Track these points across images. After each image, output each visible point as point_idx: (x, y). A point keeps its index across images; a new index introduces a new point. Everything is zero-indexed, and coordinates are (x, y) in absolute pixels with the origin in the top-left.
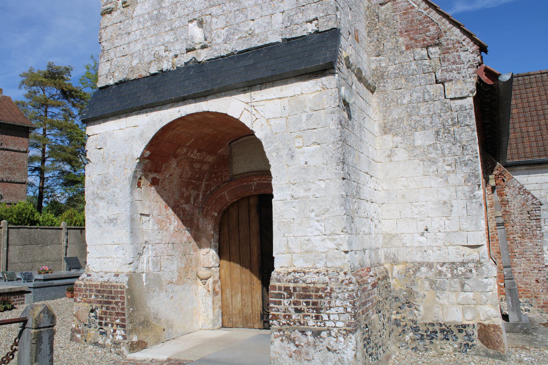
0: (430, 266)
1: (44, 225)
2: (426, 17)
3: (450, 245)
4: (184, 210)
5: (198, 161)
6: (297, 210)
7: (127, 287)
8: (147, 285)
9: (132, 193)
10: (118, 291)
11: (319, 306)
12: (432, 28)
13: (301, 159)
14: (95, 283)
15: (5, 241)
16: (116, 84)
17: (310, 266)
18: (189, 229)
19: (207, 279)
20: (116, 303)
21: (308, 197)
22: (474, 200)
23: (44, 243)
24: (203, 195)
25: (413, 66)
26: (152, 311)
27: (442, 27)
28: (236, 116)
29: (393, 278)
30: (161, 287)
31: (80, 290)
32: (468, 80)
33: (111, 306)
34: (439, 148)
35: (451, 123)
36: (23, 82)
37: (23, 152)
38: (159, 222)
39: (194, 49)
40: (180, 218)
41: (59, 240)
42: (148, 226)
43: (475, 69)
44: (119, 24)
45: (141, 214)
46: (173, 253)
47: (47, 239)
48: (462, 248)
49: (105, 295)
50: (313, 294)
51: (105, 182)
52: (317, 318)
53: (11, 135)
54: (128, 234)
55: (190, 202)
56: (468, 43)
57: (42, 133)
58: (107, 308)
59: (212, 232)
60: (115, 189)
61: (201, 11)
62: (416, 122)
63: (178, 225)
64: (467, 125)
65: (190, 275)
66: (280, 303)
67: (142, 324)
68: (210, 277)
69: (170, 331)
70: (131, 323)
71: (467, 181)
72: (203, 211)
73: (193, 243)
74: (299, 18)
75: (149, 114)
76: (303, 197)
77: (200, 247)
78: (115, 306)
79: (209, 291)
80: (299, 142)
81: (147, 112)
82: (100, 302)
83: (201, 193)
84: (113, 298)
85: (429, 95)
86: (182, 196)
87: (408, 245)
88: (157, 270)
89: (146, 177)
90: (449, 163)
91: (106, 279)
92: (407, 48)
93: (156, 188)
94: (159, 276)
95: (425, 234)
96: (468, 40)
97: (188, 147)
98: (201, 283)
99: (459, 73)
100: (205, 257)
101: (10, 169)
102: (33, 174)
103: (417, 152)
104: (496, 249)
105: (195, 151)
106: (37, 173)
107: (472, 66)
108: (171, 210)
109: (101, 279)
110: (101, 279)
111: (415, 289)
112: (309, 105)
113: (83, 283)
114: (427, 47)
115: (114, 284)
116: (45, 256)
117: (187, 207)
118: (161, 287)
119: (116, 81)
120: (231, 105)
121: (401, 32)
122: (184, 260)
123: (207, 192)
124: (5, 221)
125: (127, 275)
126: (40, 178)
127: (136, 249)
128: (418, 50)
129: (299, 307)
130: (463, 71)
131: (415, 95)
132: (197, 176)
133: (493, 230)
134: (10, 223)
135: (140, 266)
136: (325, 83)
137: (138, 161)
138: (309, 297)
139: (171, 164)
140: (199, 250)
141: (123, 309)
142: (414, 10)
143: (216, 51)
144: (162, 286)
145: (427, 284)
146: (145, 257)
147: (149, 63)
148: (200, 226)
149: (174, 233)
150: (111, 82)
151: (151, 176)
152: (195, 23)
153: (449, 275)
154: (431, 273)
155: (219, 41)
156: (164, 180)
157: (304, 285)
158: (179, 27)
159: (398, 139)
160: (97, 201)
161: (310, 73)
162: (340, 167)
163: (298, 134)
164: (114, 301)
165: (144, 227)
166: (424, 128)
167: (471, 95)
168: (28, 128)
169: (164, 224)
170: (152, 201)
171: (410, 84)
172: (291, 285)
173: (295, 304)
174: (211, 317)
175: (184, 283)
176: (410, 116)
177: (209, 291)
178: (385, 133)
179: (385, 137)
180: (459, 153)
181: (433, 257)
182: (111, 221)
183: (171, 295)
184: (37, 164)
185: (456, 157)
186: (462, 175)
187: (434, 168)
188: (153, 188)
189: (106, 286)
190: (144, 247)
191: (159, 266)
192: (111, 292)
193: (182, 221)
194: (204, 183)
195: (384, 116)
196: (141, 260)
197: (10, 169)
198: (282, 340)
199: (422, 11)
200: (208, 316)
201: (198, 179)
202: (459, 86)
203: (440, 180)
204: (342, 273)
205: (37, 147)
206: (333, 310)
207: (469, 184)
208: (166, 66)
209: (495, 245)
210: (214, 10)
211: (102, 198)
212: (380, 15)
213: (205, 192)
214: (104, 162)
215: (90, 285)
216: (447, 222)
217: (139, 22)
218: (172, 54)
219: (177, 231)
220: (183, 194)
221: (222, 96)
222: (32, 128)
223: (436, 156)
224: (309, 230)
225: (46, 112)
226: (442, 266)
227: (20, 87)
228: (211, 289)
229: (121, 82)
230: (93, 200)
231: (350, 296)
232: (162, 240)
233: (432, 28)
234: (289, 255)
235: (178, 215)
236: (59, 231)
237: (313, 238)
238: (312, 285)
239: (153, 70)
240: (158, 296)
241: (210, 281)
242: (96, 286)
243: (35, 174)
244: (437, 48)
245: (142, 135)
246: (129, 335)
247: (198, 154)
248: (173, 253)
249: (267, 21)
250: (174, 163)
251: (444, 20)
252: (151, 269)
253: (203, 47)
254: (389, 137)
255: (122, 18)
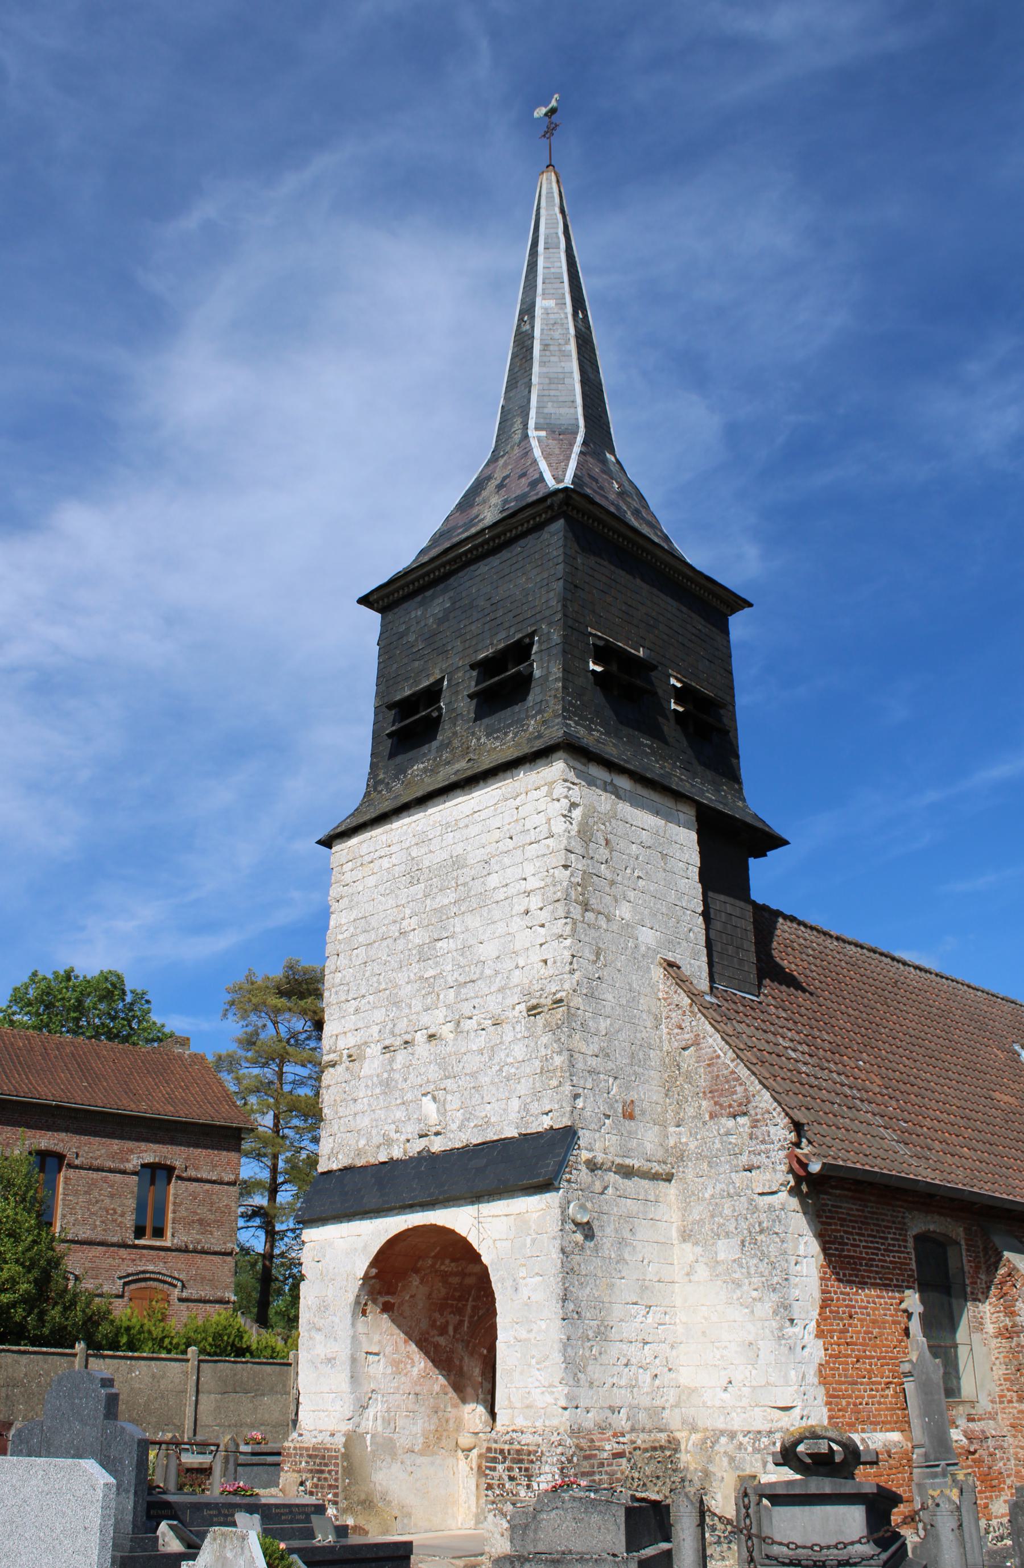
0: (732, 1435)
1: (259, 1358)
2: (733, 1072)
3: (756, 1405)
4: (436, 1346)
5: (456, 1274)
6: (519, 1355)
7: (343, 1450)
8: (372, 1451)
9: (353, 1325)
10: (332, 1456)
11: (530, 1473)
12: (739, 1089)
13: (525, 1292)
14: (306, 1445)
15: (194, 1384)
16: (340, 1170)
17: (530, 1424)
18: (444, 1372)
19: (470, 1450)
20: (329, 1472)
21: (529, 1340)
22: (783, 1342)
23: (258, 1390)
24: (469, 1322)
25: (718, 1145)
26: (378, 1487)
27: (751, 1089)
28: (464, 1234)
29: (687, 1452)
30: (394, 1455)
31: (289, 1455)
32: (778, 1168)
33: (324, 1476)
34: (745, 1265)
35: (758, 1229)
36: (232, 1003)
37: (229, 1184)
38: (395, 1364)
39: (426, 1135)
40: (429, 1358)
41: (284, 1386)
42: (378, 1369)
43: (786, 1152)
44: (344, 1085)
45: (367, 1353)
46: (416, 1407)
47: (264, 1383)
48: (769, 1410)
49: (318, 1461)
50: (525, 1457)
51: (323, 1308)
52: (529, 1486)
53: (206, 1147)
54: (348, 1379)
55: (447, 1332)
56: (779, 1114)
57: (271, 1125)
58: (319, 1479)
59: (480, 1379)
60: (334, 1318)
61: (435, 1082)
62: (720, 1226)
63: (425, 1367)
64: (777, 1233)
65: (444, 1443)
66: (494, 1469)
67: (362, 1503)
68: (474, 1448)
69: (405, 1521)
70: (345, 1499)
71: (775, 1313)
72: (467, 1346)
73: (452, 1394)
74: (535, 1108)
75: (373, 1221)
76: (525, 1340)
77: (464, 1401)
78: (327, 1475)
79: (472, 1469)
80: (523, 1272)
81: (371, 1218)
82: (311, 1471)
83: (466, 1319)
84: (326, 1465)
85: (734, 1188)
86: (433, 1324)
87: (709, 1404)
88: (388, 1431)
89: (374, 1301)
90: (756, 1287)
91: (319, 1439)
92: (711, 1117)
93: (390, 1317)
94: (391, 1439)
95: (729, 1389)
96: (779, 1109)
97: (434, 1257)
98: (462, 1457)
99: (768, 1157)
100: (470, 1416)
101: (201, 1222)
102: (250, 1224)
103: (720, 1269)
104: (1009, 1419)
105: (447, 1261)
106: (257, 1222)
107: (782, 1148)
108: (414, 1346)
109: (314, 1440)
110: (314, 1440)
111: (712, 1468)
112: (534, 1227)
113: (292, 1445)
114: (734, 1117)
115: (328, 1446)
116: (259, 1416)
117: (442, 1341)
118: (394, 1455)
119: (340, 1166)
120: (458, 1219)
121: (704, 1092)
122: (435, 1420)
123: (473, 1317)
124: (194, 1348)
125: (344, 1435)
126: (267, 1233)
127: (358, 1399)
128: (724, 1120)
129: (512, 1474)
130: (772, 1154)
131: (719, 1186)
132: (457, 1294)
133: (1002, 1382)
134: (202, 1351)
135: (363, 1424)
136: (549, 1200)
137: (361, 1282)
138: (521, 1461)
139: (411, 1282)
140: (461, 1405)
141: (336, 1480)
142: (720, 1061)
143: (451, 1140)
144: (396, 1455)
145: (725, 1460)
146: (371, 1412)
147: (378, 1147)
148: (465, 1368)
149: (419, 1379)
150: (335, 1167)
151: (382, 1300)
152: (429, 1096)
153: (750, 1449)
154: (731, 1446)
155: (454, 1126)
156: (402, 1304)
157: (518, 1447)
158: (411, 1101)
159: (699, 1250)
160: (313, 1333)
161: (534, 1187)
162: (559, 1305)
163: (522, 1261)
164: (327, 1469)
165: (372, 1370)
166: (727, 1235)
167: (784, 1189)
168: (239, 1130)
169: (402, 1366)
170: (384, 1334)
171: (713, 1171)
172: (506, 1447)
173: (509, 1471)
174: (474, 1509)
175: (434, 1454)
176: (712, 1216)
177: (472, 1469)
178: (684, 1241)
179: (684, 1246)
180: (766, 1273)
181: (737, 1423)
182: (329, 1360)
183: (409, 1469)
184: (260, 1200)
185: (764, 1279)
186: (770, 1304)
187: (738, 1293)
188: (386, 1316)
189: (319, 1449)
190: (370, 1398)
191: (392, 1425)
192: (323, 1457)
193: (433, 1361)
194: (470, 1304)
195: (683, 1215)
196: (365, 1415)
197: (201, 1222)
198: (495, 1515)
199: (729, 1062)
200: (469, 1508)
201: (460, 1299)
202: (768, 1176)
203: (746, 1310)
204: (555, 1434)
205: (259, 1156)
206: (542, 1478)
207: (778, 1318)
208: (397, 1153)
209: (1007, 1411)
210: (449, 1084)
211: (319, 1330)
212: (682, 1064)
213: (471, 1317)
214: (323, 1280)
215: (300, 1448)
216: (754, 1372)
217: (367, 1086)
218: (403, 1138)
219: (424, 1377)
220: (435, 1321)
221: (451, 1207)
222: (247, 1129)
223: (741, 1277)
224: (530, 1380)
225: (280, 1074)
226: (745, 1436)
227: (225, 1015)
228: (475, 1466)
229: (346, 1169)
230: (309, 1330)
231: (558, 1460)
232: (398, 1388)
233: (739, 1089)
234: (510, 1411)
235: (427, 1354)
236: (286, 1368)
237: (533, 1391)
238: (525, 1448)
239: (383, 1158)
240: (390, 1468)
241: (475, 1453)
242: (307, 1449)
243: (255, 1224)
244: (746, 1118)
245: (365, 1247)
246: (342, 1515)
247: (453, 1264)
248: (416, 1407)
249: (503, 1106)
250: (415, 1280)
251: (753, 1078)
252: (380, 1429)
253: (437, 1134)
254: (688, 1246)
255: (348, 1076)
